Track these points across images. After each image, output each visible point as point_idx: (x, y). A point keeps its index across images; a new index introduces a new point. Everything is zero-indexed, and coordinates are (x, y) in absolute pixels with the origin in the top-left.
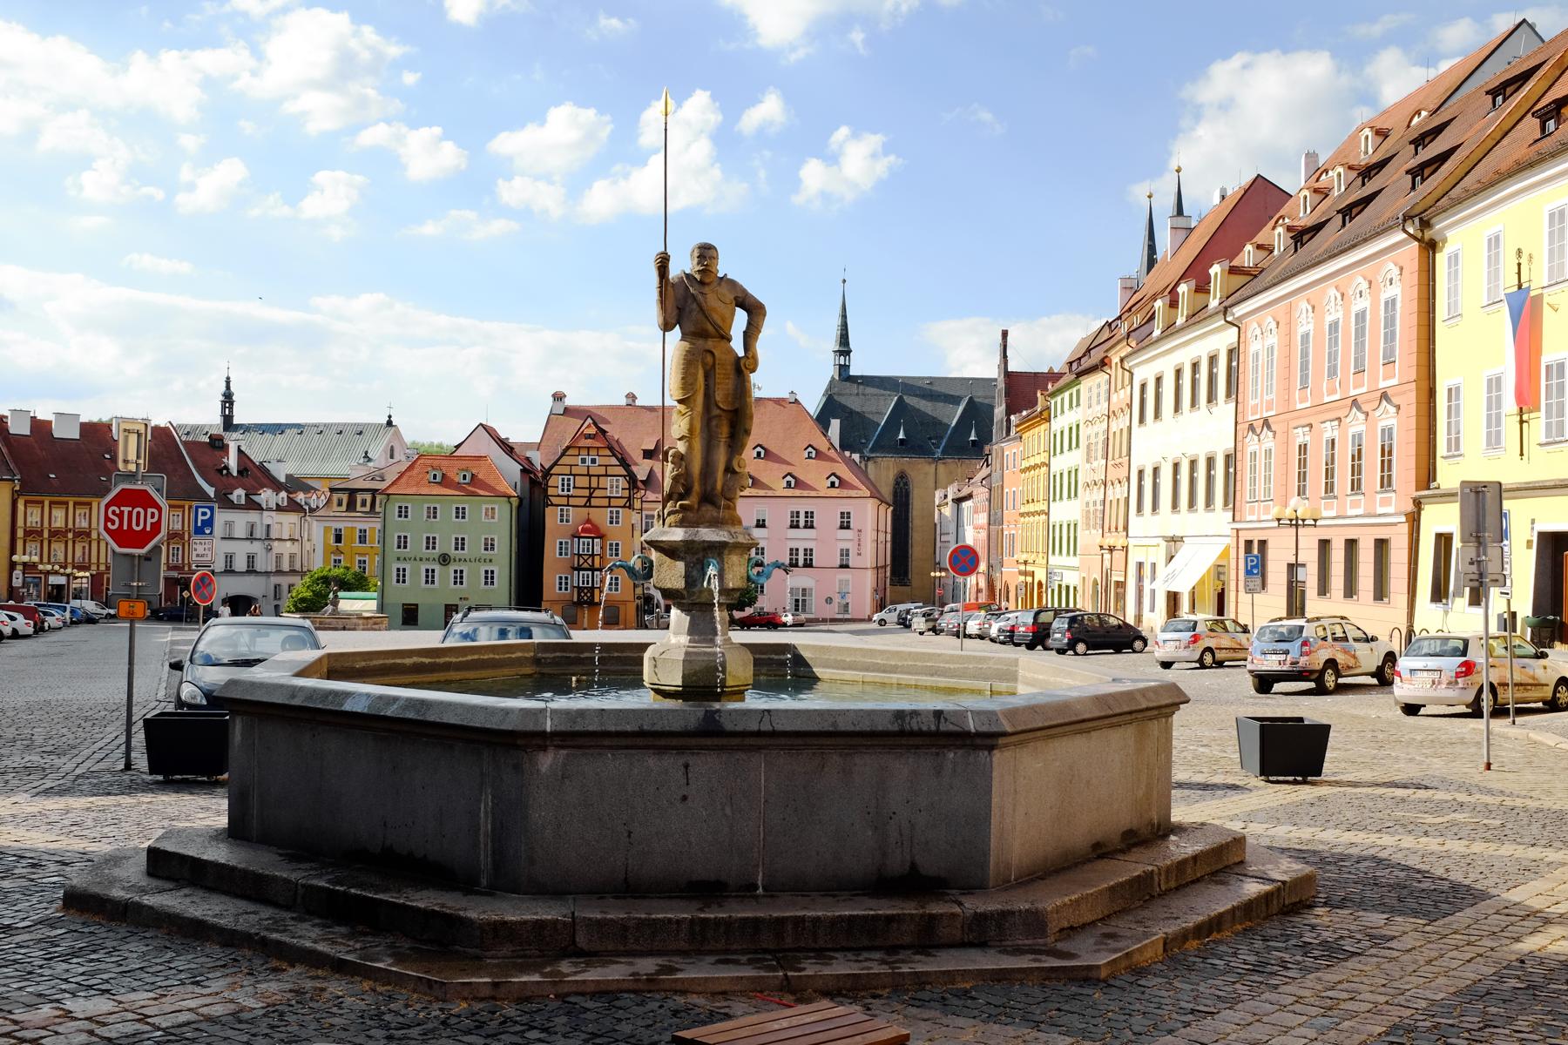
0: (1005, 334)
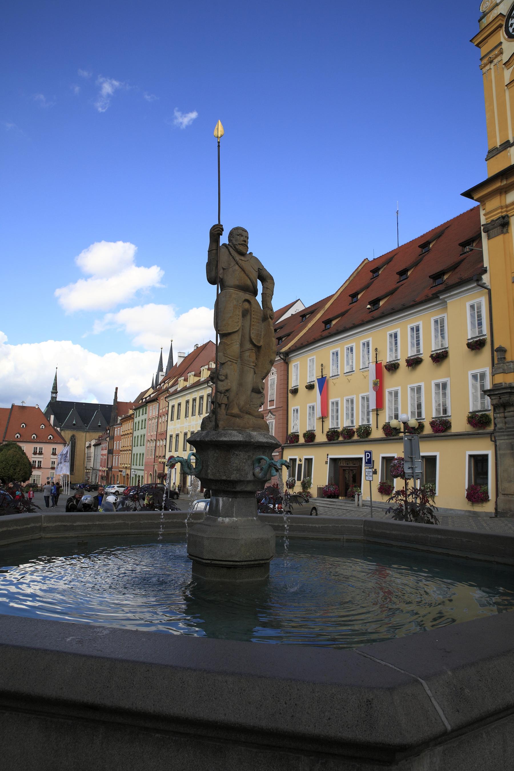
0: (117, 389)
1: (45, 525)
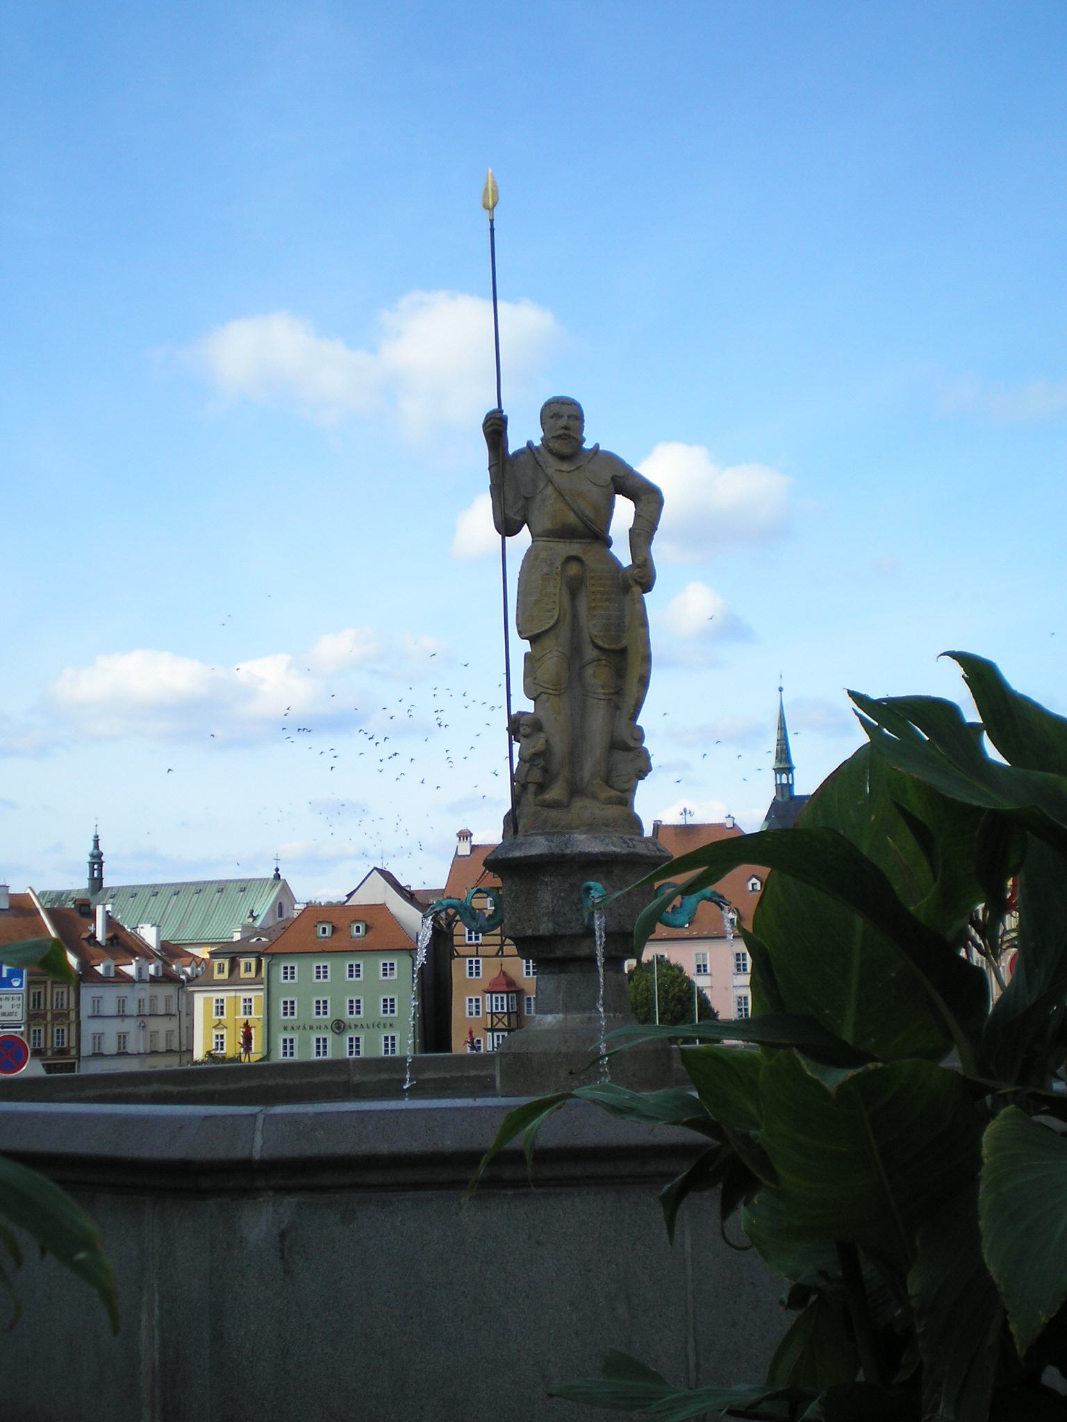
1: (357, 1078)
